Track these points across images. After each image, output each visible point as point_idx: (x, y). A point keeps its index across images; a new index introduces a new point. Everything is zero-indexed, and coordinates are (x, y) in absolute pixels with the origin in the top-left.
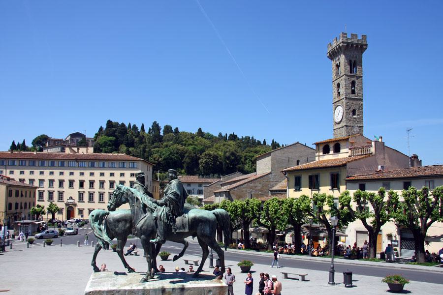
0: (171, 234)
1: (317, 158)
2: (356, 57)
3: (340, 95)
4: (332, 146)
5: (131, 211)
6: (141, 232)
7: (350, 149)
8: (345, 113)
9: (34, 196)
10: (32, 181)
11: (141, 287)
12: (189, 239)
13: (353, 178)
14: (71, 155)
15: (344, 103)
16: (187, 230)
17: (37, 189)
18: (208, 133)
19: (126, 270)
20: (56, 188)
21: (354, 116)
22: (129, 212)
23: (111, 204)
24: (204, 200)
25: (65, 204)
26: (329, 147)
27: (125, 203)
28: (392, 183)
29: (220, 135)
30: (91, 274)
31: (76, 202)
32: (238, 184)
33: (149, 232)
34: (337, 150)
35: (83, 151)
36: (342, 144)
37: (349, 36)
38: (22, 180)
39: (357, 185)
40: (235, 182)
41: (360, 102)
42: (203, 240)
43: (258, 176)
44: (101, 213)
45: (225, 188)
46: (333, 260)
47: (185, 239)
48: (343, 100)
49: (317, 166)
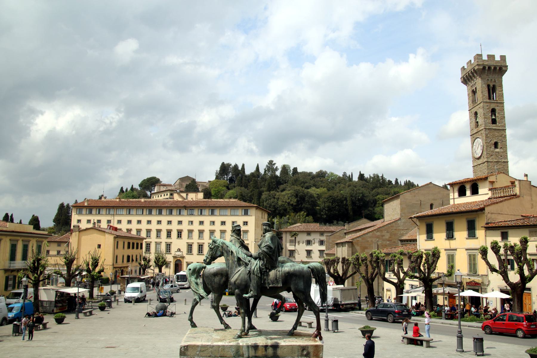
0: (264, 290)
1: (452, 202)
2: (495, 81)
3: (478, 126)
5: (226, 264)
6: (237, 285)
7: (490, 190)
8: (485, 147)
9: (141, 248)
10: (139, 231)
11: (233, 343)
12: (284, 294)
13: (494, 225)
14: (180, 201)
15: (484, 135)
16: (280, 285)
17: (145, 240)
18: (332, 174)
19: (222, 327)
20: (164, 238)
22: (224, 266)
23: (207, 258)
24: (325, 252)
25: (174, 257)
27: (220, 256)
29: (345, 174)
30: (188, 329)
31: (185, 255)
32: (370, 230)
33: (244, 287)
34: (475, 192)
35: (192, 197)
36: (480, 185)
37: (485, 58)
38: (129, 231)
39: (499, 232)
40: (361, 230)
41: (503, 132)
42: (297, 295)
43: (386, 223)
44: (198, 267)
45: (348, 238)
46: (460, 323)
47: (281, 294)
48: (482, 132)
49: (451, 210)
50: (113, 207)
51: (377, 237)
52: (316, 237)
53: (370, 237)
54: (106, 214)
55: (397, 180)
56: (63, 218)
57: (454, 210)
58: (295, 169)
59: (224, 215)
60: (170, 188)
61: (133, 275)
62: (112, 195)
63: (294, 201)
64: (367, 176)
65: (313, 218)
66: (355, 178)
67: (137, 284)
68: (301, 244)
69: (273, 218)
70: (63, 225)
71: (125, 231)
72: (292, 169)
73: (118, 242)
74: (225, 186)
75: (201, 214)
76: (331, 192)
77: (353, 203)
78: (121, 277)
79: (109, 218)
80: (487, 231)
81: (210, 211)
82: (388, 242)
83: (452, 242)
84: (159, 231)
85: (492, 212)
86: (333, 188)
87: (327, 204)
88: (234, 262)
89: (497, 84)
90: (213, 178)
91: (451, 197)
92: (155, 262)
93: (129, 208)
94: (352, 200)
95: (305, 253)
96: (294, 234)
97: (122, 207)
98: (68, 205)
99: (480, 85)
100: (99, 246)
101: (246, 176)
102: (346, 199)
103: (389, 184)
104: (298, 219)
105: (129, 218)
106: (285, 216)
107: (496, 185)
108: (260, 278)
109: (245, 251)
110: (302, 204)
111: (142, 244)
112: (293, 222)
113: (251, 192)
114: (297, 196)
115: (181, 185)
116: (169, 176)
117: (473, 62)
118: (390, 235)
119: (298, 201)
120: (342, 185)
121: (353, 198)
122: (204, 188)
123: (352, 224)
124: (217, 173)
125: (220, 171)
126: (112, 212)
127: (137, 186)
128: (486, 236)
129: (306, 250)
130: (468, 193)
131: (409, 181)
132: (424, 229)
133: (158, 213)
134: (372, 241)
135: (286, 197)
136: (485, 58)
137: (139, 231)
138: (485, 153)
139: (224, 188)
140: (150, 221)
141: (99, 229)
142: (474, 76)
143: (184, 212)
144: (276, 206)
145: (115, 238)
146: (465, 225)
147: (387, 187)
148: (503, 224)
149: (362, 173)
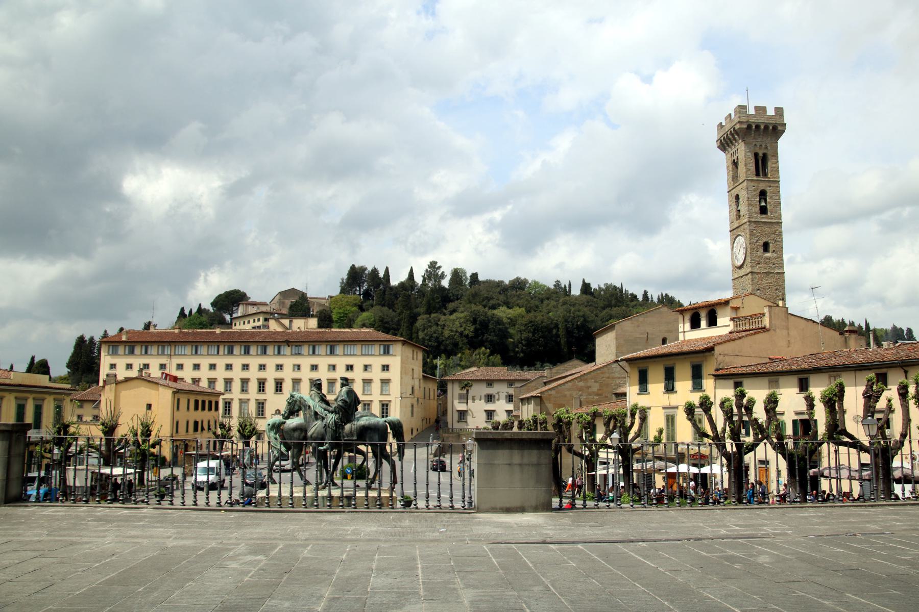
2: (766, 148)
4: (703, 315)
7: (732, 319)
9: (217, 409)
10: (212, 381)
17: (222, 397)
20: (253, 393)
21: (767, 255)
26: (699, 315)
28: (782, 380)
29: (558, 284)
34: (712, 322)
35: (299, 324)
36: (719, 312)
38: (196, 381)
39: (731, 383)
41: (777, 227)
48: (746, 226)
50: (170, 343)
51: (580, 389)
52: (502, 390)
53: (569, 390)
54: (158, 354)
55: (646, 292)
56: (85, 360)
57: (685, 349)
58: (474, 276)
59: (351, 355)
60: (263, 309)
61: (204, 451)
62: (165, 321)
63: (470, 329)
64: (594, 286)
65: (502, 359)
66: (576, 291)
67: (213, 463)
68: (477, 401)
69: (435, 358)
70: (83, 372)
71: (190, 382)
72: (468, 275)
73: (178, 400)
74: (355, 305)
75: (314, 352)
76: (532, 314)
77: (569, 333)
78: (185, 454)
79: (164, 360)
80: (718, 381)
81: (329, 348)
82: (596, 397)
83: (672, 396)
84: (245, 382)
85: (726, 352)
86: (537, 307)
87: (524, 335)
88: (311, 416)
89: (769, 153)
90: (336, 291)
91: (681, 330)
92: (239, 431)
93: (196, 344)
94: (567, 329)
95: (484, 415)
96: (466, 385)
97: (185, 343)
98: (92, 339)
99: (743, 153)
100: (149, 406)
101: (392, 288)
102: (557, 326)
103: (632, 301)
104: (476, 359)
105: (196, 360)
106: (456, 355)
107: (742, 313)
108: (335, 431)
109: (324, 406)
110: (483, 334)
111: (217, 403)
112: (468, 364)
113: (400, 314)
114: (474, 321)
115: (282, 303)
116: (263, 290)
117: (733, 116)
118: (600, 386)
119: (476, 330)
120: (553, 303)
121: (569, 325)
122: (321, 308)
123: (555, 369)
124: (343, 283)
125: (348, 279)
126: (167, 350)
127: (207, 305)
128: (715, 388)
129: (486, 411)
130: (703, 323)
131: (666, 295)
132: (635, 377)
133: (243, 352)
134: (571, 395)
135: (457, 323)
136: (752, 111)
137: (212, 381)
138: (748, 259)
139: (355, 309)
140: (231, 365)
141: (149, 379)
142: (735, 139)
143: (287, 350)
144: (441, 339)
145: (174, 393)
146: (662, 375)
147: (627, 306)
148: (736, 371)
149: (587, 281)
